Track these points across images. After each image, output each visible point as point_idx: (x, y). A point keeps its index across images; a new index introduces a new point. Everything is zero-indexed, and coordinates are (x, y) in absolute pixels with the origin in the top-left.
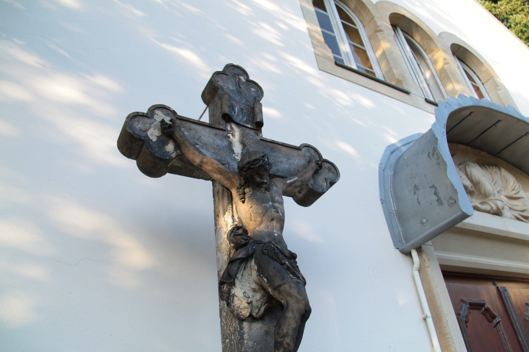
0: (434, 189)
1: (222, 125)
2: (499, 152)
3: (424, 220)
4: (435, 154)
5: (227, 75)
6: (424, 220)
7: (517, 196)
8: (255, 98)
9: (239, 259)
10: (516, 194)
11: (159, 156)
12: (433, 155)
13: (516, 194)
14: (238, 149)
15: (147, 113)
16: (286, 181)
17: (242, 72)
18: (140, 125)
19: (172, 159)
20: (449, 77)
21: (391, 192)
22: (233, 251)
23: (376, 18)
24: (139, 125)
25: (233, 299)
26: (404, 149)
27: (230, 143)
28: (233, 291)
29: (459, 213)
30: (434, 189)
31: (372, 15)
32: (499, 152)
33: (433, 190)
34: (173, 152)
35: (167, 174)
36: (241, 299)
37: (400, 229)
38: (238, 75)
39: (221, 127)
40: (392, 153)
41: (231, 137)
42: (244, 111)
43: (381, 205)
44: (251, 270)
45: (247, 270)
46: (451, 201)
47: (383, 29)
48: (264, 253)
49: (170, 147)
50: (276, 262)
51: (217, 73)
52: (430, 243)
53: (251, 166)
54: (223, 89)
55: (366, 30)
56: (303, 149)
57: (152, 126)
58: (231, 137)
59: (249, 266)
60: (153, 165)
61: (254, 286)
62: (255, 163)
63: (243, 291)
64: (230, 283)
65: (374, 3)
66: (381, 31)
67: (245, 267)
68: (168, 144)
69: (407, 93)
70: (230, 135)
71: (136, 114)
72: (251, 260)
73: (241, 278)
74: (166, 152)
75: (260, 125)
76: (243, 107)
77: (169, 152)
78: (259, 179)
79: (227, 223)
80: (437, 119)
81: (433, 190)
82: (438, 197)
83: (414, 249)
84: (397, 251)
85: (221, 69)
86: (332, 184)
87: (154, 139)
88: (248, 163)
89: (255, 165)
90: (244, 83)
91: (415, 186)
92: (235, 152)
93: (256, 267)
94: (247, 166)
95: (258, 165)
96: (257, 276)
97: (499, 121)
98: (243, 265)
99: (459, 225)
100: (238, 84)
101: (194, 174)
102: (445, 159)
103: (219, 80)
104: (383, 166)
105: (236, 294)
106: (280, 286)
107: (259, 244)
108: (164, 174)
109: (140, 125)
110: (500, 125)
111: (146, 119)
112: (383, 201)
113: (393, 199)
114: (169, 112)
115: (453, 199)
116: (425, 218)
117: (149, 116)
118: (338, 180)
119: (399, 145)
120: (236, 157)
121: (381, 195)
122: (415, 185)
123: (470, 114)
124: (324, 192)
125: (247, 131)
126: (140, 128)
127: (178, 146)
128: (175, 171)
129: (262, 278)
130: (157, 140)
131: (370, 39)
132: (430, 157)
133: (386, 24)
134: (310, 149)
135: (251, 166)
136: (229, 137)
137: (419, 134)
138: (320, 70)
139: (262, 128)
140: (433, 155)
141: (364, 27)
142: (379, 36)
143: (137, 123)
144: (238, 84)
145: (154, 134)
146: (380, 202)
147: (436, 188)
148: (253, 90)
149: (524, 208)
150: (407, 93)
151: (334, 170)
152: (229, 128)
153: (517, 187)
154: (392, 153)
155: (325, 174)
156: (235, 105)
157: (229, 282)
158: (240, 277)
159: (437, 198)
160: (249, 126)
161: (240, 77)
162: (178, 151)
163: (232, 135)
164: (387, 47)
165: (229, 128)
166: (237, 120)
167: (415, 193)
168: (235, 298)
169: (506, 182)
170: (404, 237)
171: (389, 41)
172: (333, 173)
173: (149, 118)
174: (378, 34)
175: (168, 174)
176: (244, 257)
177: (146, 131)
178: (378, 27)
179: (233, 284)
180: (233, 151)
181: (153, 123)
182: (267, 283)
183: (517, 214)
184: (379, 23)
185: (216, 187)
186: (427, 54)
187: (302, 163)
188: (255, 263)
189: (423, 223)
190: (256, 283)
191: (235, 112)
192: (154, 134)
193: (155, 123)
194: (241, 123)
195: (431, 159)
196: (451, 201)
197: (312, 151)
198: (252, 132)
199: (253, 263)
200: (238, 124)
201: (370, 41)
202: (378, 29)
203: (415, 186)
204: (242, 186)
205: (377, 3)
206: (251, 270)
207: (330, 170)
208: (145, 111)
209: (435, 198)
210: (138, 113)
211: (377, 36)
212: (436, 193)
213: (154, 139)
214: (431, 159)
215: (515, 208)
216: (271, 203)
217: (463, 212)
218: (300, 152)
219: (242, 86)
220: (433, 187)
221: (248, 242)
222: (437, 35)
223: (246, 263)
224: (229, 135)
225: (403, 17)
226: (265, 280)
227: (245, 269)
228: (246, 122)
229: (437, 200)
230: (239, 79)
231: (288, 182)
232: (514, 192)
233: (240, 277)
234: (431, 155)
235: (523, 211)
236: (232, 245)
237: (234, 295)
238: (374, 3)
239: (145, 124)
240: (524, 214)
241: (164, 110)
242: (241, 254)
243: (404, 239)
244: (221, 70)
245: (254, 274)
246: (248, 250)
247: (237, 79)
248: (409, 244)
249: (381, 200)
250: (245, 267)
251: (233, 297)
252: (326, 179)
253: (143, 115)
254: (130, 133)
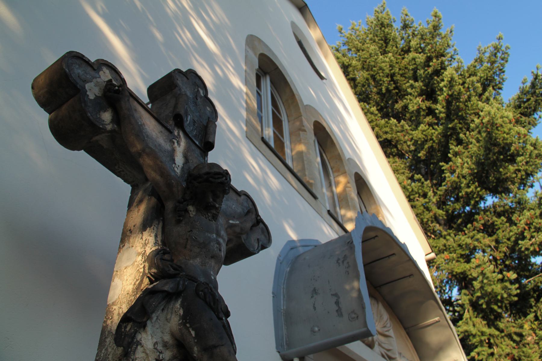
0: (336, 298)
1: (170, 125)
2: (380, 286)
3: (316, 329)
4: (345, 262)
5: (188, 79)
6: (316, 329)
7: (387, 333)
8: (209, 118)
9: (165, 291)
10: (386, 331)
11: (91, 118)
12: (343, 262)
13: (386, 331)
14: (179, 160)
15: (93, 63)
16: (229, 220)
17: (202, 85)
18: (79, 71)
19: (104, 130)
20: (348, 200)
21: (283, 288)
22: (146, 281)
23: (303, 118)
24: (78, 71)
25: (136, 348)
26: (301, 250)
27: (174, 150)
28: (139, 337)
29: (364, 329)
30: (336, 298)
31: (300, 113)
32: (380, 286)
33: (335, 299)
34: (109, 124)
35: (83, 151)
36: (148, 352)
37: (285, 331)
38: (198, 87)
39: (169, 127)
40: (292, 249)
41: (176, 144)
42: (196, 125)
43: (272, 298)
44: (172, 313)
45: (165, 312)
46: (354, 316)
47: (307, 130)
48: (198, 295)
49: (107, 116)
50: (212, 312)
51: (178, 71)
52: (311, 356)
53: (211, 179)
54: (180, 90)
55: (289, 125)
56: (243, 197)
57: (95, 80)
58: (176, 144)
59: (171, 307)
60: (69, 133)
61: (167, 338)
62: (217, 176)
63: (155, 340)
64: (140, 323)
65: (305, 104)
66: (305, 131)
67: (165, 307)
68: (105, 111)
69: (315, 197)
70: (175, 141)
71: (80, 56)
72: (176, 300)
73: (155, 322)
74: (100, 118)
75: (209, 146)
76: (196, 119)
77: (104, 121)
78: (211, 200)
79: (477, 136)
80: (356, 227)
81: (335, 299)
82: (339, 307)
83: (297, 357)
84: (278, 354)
85: (184, 70)
86: (263, 247)
87: (92, 97)
88: (208, 173)
89: (215, 179)
90: (201, 97)
91: (315, 290)
92: (176, 162)
93: (181, 312)
94: (205, 177)
95: (219, 180)
96: (180, 325)
97: (394, 254)
98: (163, 303)
99: (339, 348)
100: (196, 95)
101: (116, 167)
102: (359, 270)
103: (179, 79)
104: (281, 259)
105: (143, 342)
106: (215, 347)
107: (193, 281)
108: (79, 150)
109: (79, 71)
110: (393, 258)
111: (89, 69)
112: (275, 295)
113: (284, 297)
114: (118, 78)
115: (355, 314)
116: (318, 327)
117: (95, 68)
118: (270, 246)
119: (298, 244)
120: (176, 169)
121: (274, 288)
122: (315, 288)
123: (374, 238)
124: (254, 254)
125: (194, 147)
126: (79, 74)
127: (117, 119)
128: (95, 152)
129: (187, 328)
130: (95, 99)
131: (291, 134)
132: (339, 263)
133: (309, 127)
134: (249, 200)
135: (211, 179)
136: (174, 143)
137: (317, 241)
138: (247, 137)
139: (209, 153)
140: (343, 262)
141: (289, 122)
142: (301, 135)
143: (77, 66)
144: (196, 95)
145: (92, 90)
146: (272, 295)
147: (339, 298)
148: (208, 109)
149: (390, 348)
150: (315, 197)
151: (266, 234)
152: (176, 134)
153: (388, 325)
154: (292, 249)
155: (256, 235)
156: (189, 113)
157: (139, 321)
158: (155, 318)
159: (337, 308)
160: (197, 143)
161: (200, 89)
162: (116, 126)
163: (178, 142)
164: (302, 148)
165: (176, 134)
166: (188, 130)
167: (312, 297)
168: (139, 347)
169: (381, 317)
170: (286, 341)
171: (306, 144)
172: (265, 236)
173: (94, 70)
174: (301, 132)
175: (82, 153)
176: (171, 291)
177: (85, 81)
178: (303, 126)
179: (143, 326)
180: (174, 160)
181: (96, 78)
182: (195, 338)
183: (383, 351)
184: (305, 123)
185: (137, 194)
186: (333, 172)
187: (239, 211)
188: (182, 306)
189: (313, 331)
190: (173, 335)
191: (187, 120)
192: (92, 90)
193: (99, 80)
194: (190, 135)
195: (339, 265)
196: (354, 316)
197: (250, 203)
198: (198, 151)
199: (178, 305)
200: (186, 134)
201: (290, 136)
202: (303, 128)
203: (315, 290)
204: (185, 201)
205: (307, 105)
206: (172, 313)
207: (263, 232)
208: (93, 60)
209: (335, 308)
210: (84, 56)
211: (299, 135)
212: (337, 303)
213: (92, 97)
214: (339, 265)
215: (383, 345)
216: (215, 236)
217: (368, 329)
218: (239, 198)
219: (199, 99)
220: (336, 295)
221: (179, 274)
222: (347, 158)
223: (168, 302)
224: (174, 140)
225: (324, 128)
226: (193, 333)
227: (163, 310)
228: (195, 136)
229: (337, 311)
230: (198, 91)
231: (231, 222)
232: (386, 329)
233: (155, 318)
234: (340, 262)
235: (389, 350)
236: (154, 270)
237: (139, 343)
238: (305, 104)
239: (86, 73)
240: (389, 353)
241: (113, 72)
242: (168, 286)
243: (286, 344)
244: (184, 70)
245: (175, 322)
246: (178, 284)
247: (196, 90)
248: (294, 350)
249: (273, 293)
250: (165, 307)
251: (137, 346)
252: (258, 239)
253: (87, 62)
254: (65, 72)
